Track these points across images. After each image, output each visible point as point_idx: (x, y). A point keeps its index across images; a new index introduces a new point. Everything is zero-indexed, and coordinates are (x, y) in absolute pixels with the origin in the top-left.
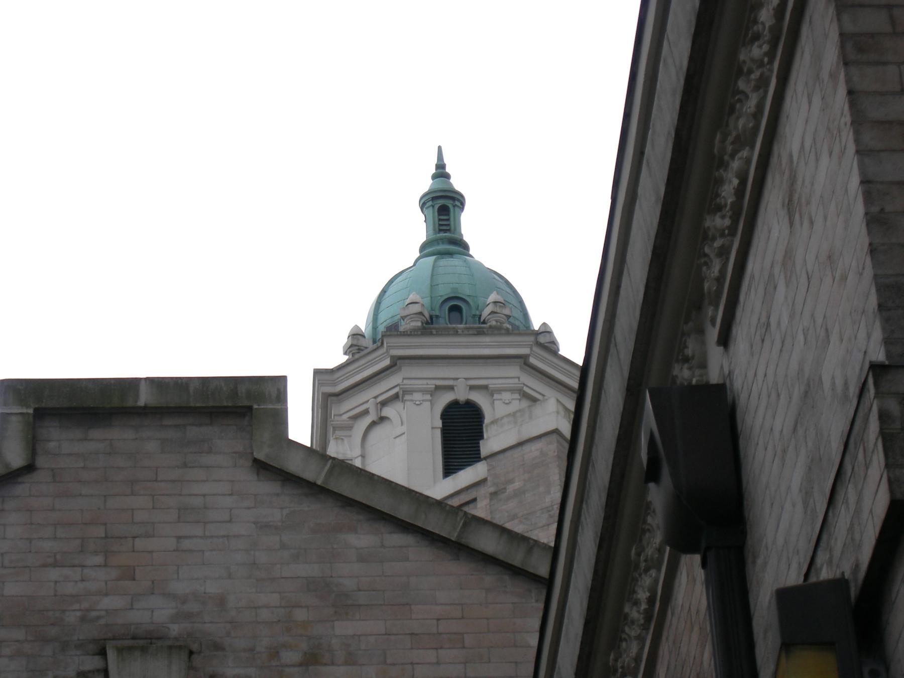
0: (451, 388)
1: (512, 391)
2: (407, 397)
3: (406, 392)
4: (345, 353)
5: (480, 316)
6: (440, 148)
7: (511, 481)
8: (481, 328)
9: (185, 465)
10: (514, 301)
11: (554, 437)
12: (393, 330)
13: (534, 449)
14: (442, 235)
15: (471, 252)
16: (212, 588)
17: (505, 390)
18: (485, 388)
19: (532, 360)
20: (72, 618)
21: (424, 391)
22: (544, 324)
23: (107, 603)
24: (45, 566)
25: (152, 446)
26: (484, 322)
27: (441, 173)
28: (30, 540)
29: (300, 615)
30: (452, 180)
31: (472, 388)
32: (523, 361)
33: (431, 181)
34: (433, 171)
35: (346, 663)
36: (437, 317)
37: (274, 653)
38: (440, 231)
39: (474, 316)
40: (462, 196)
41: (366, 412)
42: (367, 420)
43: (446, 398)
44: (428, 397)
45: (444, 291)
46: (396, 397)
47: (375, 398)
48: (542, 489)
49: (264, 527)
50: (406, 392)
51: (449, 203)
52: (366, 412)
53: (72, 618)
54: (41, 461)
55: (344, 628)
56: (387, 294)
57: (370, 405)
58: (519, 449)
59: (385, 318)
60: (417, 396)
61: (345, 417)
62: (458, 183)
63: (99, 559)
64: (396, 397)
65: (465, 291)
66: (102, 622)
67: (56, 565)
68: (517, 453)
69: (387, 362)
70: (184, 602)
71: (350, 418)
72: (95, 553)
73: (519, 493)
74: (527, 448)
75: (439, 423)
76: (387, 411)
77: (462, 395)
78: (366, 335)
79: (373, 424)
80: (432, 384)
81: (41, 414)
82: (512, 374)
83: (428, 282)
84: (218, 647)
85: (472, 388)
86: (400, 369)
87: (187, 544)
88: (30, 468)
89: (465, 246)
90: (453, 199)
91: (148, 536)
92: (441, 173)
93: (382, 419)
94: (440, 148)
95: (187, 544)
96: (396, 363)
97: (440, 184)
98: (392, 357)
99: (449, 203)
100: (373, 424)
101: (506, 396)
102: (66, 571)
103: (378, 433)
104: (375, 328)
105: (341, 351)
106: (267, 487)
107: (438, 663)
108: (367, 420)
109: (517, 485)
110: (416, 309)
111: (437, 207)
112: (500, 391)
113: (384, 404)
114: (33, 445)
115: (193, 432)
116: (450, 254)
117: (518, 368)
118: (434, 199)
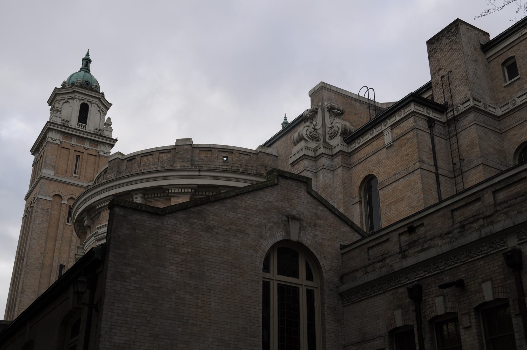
0: (84, 100)
1: (96, 104)
2: (74, 99)
3: (74, 98)
4: (61, 86)
5: (92, 87)
6: (89, 49)
7: (181, 151)
8: (92, 90)
9: (298, 189)
10: (98, 86)
11: (191, 146)
12: (73, 84)
13: (186, 147)
14: (86, 67)
15: (91, 72)
16: (302, 211)
17: (95, 104)
18: (90, 102)
19: (101, 99)
20: (284, 211)
21: (78, 99)
22: (103, 92)
23: (288, 209)
24: (280, 201)
25: (294, 185)
26: (92, 88)
27: (88, 54)
28: (278, 196)
29: (313, 218)
30: (90, 57)
31: (88, 101)
32: (99, 99)
33: (85, 56)
34: (86, 54)
35: (319, 227)
36: (83, 84)
37: (310, 223)
38: (86, 66)
39: (91, 87)
40: (91, 60)
41: (64, 99)
42: (64, 101)
43: (83, 102)
44: (79, 100)
45: (86, 80)
46: (72, 98)
47: (67, 97)
48: (187, 154)
49: (308, 202)
50: (74, 98)
51: (89, 61)
52: (64, 99)
53: (284, 211)
54: (279, 183)
55: (319, 221)
56: (73, 76)
57: (66, 98)
58: (183, 146)
59: (71, 81)
60: (77, 100)
61: (59, 99)
62: (91, 57)
63: (287, 202)
64: (72, 98)
65: (90, 81)
66: (288, 212)
67: (281, 201)
68: (183, 147)
69: (72, 91)
70: (298, 212)
71: (61, 99)
72: (287, 201)
73: (182, 154)
74: (185, 146)
75: (80, 106)
76: (69, 100)
77: (86, 102)
78: (67, 82)
79: (65, 102)
80: (80, 98)
81: (279, 175)
82: (97, 101)
83: (83, 77)
84: (303, 220)
85: (88, 101)
86: (74, 93)
87: (299, 202)
88: (277, 184)
89: (90, 71)
90: (90, 61)
91: (294, 200)
92: (88, 54)
93: (68, 102)
94: (89, 49)
95: (299, 202)
96: (74, 92)
97: (87, 57)
98: (74, 90)
99: (89, 61)
100: (65, 102)
101: (95, 105)
102: (283, 203)
103: (65, 104)
104: (69, 82)
105: (60, 85)
106: (309, 196)
107: (330, 230)
108: (64, 101)
109: (182, 152)
110: (80, 82)
111: (86, 61)
112: (93, 103)
113: (69, 99)
114: (278, 181)
115: (299, 184)
116: (87, 72)
117: (98, 100)
118: (86, 60)
